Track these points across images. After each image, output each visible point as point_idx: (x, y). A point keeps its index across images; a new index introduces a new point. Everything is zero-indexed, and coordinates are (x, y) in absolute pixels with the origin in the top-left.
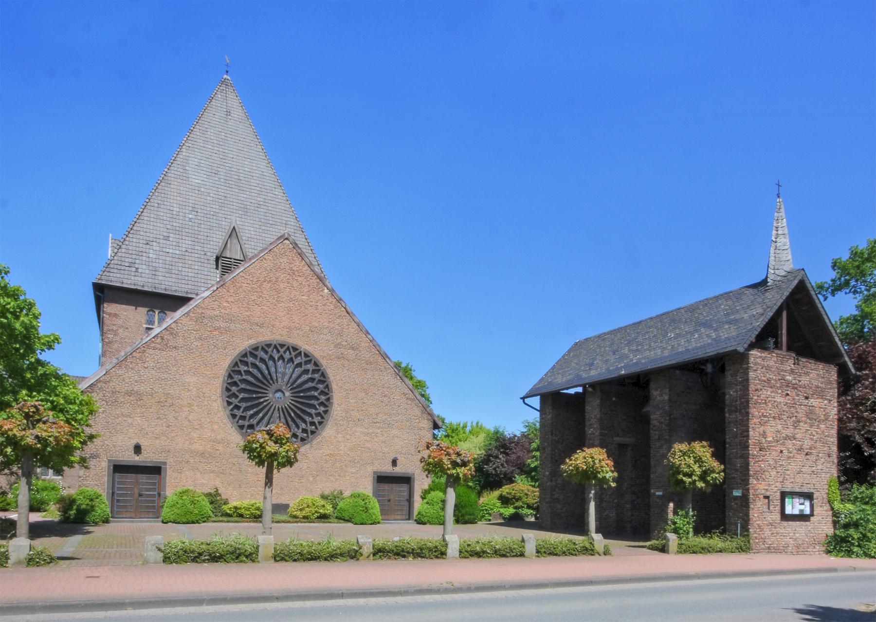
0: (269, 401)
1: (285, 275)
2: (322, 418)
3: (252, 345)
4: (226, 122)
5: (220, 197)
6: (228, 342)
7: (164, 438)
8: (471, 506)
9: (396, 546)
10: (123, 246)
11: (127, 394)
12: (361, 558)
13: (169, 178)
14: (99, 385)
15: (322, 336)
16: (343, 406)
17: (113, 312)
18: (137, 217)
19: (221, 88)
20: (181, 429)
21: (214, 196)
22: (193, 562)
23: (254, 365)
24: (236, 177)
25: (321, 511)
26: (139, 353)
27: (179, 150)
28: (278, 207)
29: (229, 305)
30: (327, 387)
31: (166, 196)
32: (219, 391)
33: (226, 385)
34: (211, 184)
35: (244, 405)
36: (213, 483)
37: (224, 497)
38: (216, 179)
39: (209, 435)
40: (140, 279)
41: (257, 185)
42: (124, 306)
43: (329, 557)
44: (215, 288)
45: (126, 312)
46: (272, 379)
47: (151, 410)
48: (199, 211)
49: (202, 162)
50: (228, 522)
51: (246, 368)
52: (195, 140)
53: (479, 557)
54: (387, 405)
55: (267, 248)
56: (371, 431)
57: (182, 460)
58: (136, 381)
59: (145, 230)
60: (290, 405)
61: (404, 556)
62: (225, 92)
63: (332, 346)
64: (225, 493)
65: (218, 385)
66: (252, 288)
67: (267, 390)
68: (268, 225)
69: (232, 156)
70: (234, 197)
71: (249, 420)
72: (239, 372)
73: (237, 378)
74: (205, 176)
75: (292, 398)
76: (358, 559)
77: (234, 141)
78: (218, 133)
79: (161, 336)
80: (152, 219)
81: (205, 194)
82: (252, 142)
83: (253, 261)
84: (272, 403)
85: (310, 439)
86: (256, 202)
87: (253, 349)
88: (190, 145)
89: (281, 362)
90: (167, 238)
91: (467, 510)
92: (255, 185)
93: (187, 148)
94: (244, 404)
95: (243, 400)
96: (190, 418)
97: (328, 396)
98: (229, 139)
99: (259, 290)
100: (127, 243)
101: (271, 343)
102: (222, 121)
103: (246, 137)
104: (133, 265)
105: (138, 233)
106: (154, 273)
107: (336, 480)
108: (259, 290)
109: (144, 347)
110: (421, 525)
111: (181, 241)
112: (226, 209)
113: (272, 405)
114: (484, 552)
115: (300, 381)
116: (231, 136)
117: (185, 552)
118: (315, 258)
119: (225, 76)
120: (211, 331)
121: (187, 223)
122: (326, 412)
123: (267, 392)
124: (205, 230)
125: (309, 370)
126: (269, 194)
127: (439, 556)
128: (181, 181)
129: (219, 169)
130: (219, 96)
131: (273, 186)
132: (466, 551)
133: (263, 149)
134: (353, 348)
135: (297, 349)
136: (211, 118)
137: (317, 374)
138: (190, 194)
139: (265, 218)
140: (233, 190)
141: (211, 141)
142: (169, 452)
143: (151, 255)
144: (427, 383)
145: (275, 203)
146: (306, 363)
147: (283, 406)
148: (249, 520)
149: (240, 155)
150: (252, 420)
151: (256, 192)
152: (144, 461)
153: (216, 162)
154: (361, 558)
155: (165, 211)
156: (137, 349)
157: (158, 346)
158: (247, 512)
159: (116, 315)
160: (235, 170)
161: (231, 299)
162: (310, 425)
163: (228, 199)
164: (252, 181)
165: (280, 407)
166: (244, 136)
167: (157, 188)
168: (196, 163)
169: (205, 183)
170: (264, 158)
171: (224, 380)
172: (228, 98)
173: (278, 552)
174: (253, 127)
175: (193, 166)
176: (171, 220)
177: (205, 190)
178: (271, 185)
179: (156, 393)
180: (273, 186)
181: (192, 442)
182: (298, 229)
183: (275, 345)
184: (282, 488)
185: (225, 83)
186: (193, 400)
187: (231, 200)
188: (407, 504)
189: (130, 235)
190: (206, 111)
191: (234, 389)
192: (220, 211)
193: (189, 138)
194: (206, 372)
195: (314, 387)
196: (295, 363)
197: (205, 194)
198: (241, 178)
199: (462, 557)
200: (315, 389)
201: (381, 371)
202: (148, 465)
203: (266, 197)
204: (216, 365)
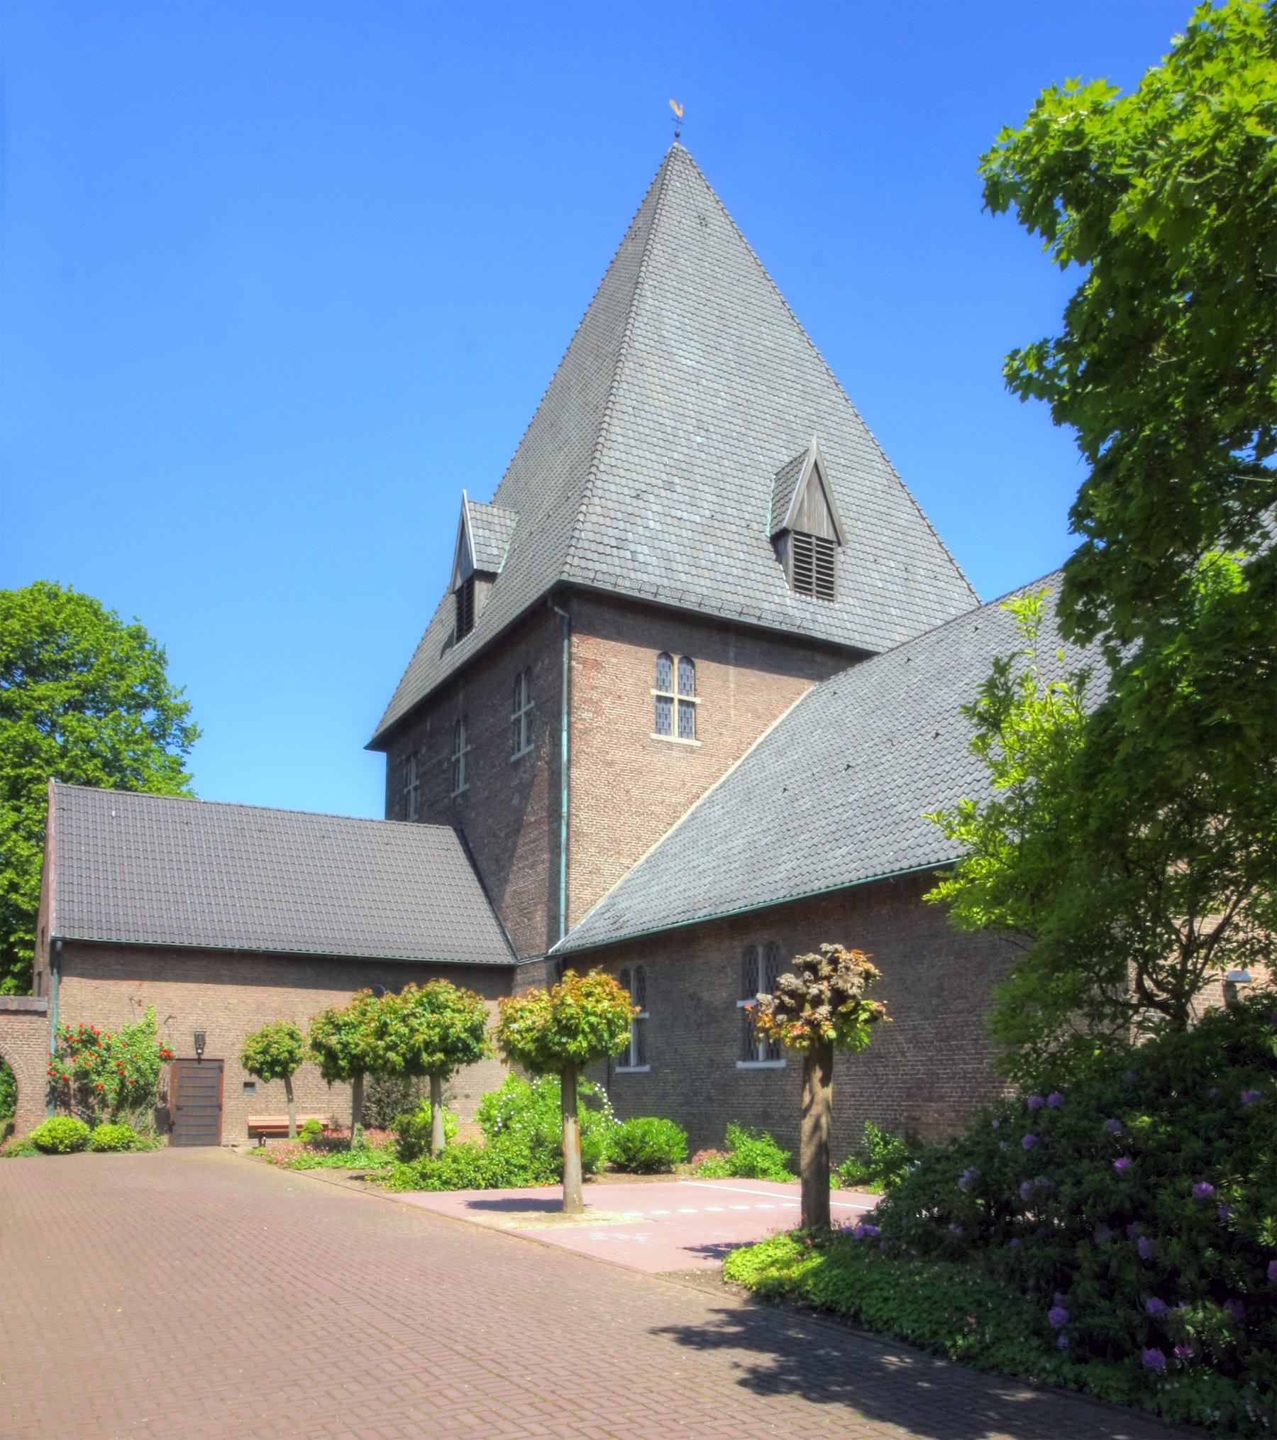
17: (590, 656)
42: (613, 643)
45: (615, 656)
74: (701, 353)
118: (940, 544)
159: (597, 665)
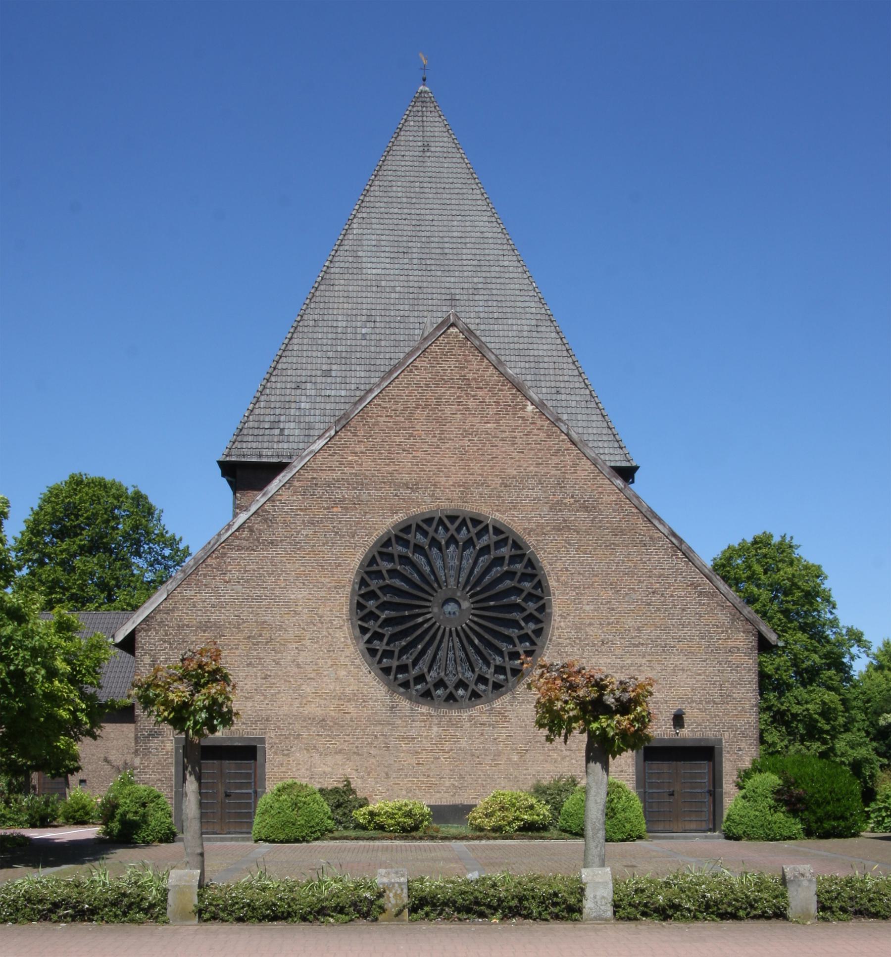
0: (434, 620)
1: (452, 390)
2: (533, 643)
3: (400, 523)
4: (421, 164)
5: (411, 290)
6: (358, 523)
7: (259, 697)
8: (838, 800)
9: (463, 893)
10: (263, 398)
11: (200, 628)
12: (381, 917)
13: (332, 276)
14: (158, 617)
15: (525, 492)
16: (570, 618)
18: (283, 347)
19: (415, 109)
20: (286, 681)
21: (402, 290)
22: (45, 920)
23: (404, 559)
24: (438, 251)
25: (526, 817)
26: (217, 558)
27: (347, 227)
28: (508, 287)
29: (357, 458)
30: (539, 585)
31: (327, 306)
32: (345, 609)
33: (356, 598)
34: (397, 272)
35: (388, 631)
36: (341, 771)
37: (360, 794)
38: (406, 261)
39: (332, 687)
40: (286, 446)
41: (473, 257)
43: (310, 913)
44: (333, 433)
46: (437, 580)
47: (237, 652)
48: (378, 319)
49: (383, 237)
50: (357, 838)
51: (390, 566)
52: (372, 205)
53: (665, 919)
54: (659, 610)
55: (418, 349)
56: (629, 661)
57: (290, 734)
58: (213, 606)
59: (294, 366)
60: (472, 625)
61: (482, 915)
62: (420, 114)
63: (546, 509)
64: (360, 786)
65: (343, 600)
66: (396, 423)
67: (430, 601)
68: (491, 321)
69: (431, 218)
70: (434, 285)
71: (399, 658)
72: (378, 574)
73: (374, 584)
74: (388, 260)
75: (473, 611)
76: (376, 920)
77: (434, 191)
78: (408, 185)
79: (248, 526)
80: (305, 348)
81: (388, 290)
82: (464, 186)
83: (395, 375)
84: (438, 624)
85: (510, 684)
86: (470, 286)
87: (401, 531)
88: (365, 215)
89: (452, 548)
90: (327, 373)
91: (829, 808)
92: (469, 257)
93: (360, 221)
94: (390, 628)
95: (388, 622)
96: (300, 660)
97: (541, 603)
98: (427, 190)
99: (407, 424)
100: (268, 391)
101: (433, 515)
102: (416, 164)
103: (455, 181)
104: (276, 425)
105: (284, 373)
106: (307, 432)
107: (563, 758)
108: (407, 424)
109: (223, 548)
110: (732, 842)
111: (348, 374)
112: (421, 308)
113: (439, 627)
114: (677, 907)
115: (487, 579)
116: (429, 185)
117: (29, 900)
119: (421, 88)
120: (328, 508)
121: (358, 343)
122: (539, 632)
123: (428, 604)
124: (388, 350)
125: (503, 558)
126: (493, 269)
127: (565, 914)
128: (350, 277)
129: (410, 244)
130: (412, 123)
131: (501, 253)
132: (630, 905)
133: (482, 194)
134: (586, 509)
135: (480, 522)
136: (398, 163)
137: (520, 562)
138: (364, 295)
139: (487, 309)
140: (433, 273)
141: (399, 200)
142: (267, 720)
143: (303, 405)
144: (823, 569)
145: (502, 280)
146: (499, 544)
147: (459, 628)
148: (393, 835)
149: (446, 212)
150: (405, 657)
151: (470, 268)
152: (229, 739)
153: (405, 233)
154: (381, 917)
155: (325, 330)
156: (213, 552)
157: (245, 543)
158: (390, 821)
160: (436, 240)
161: (360, 448)
162: (510, 659)
163: (425, 290)
164: (464, 251)
165: (453, 629)
166: (451, 180)
167: (313, 296)
168: (374, 243)
169: (387, 272)
170: (485, 208)
171: (353, 589)
172: (425, 124)
173: (206, 902)
174: (466, 161)
175: (369, 248)
176: (334, 342)
177: (389, 284)
178: (496, 252)
179: (244, 622)
180: (501, 253)
181: (304, 701)
182: (543, 317)
183: (440, 519)
184: (462, 777)
185: (420, 99)
186: (303, 629)
187: (429, 291)
188: (707, 799)
189: (273, 379)
190: (391, 153)
191: (371, 604)
192: (411, 314)
193: (363, 205)
194: (323, 580)
195: (515, 588)
196: (478, 548)
197: (388, 290)
198: (446, 251)
199: (621, 918)
200: (518, 591)
201: (645, 545)
202: (236, 744)
203: (488, 275)
204: (340, 565)
